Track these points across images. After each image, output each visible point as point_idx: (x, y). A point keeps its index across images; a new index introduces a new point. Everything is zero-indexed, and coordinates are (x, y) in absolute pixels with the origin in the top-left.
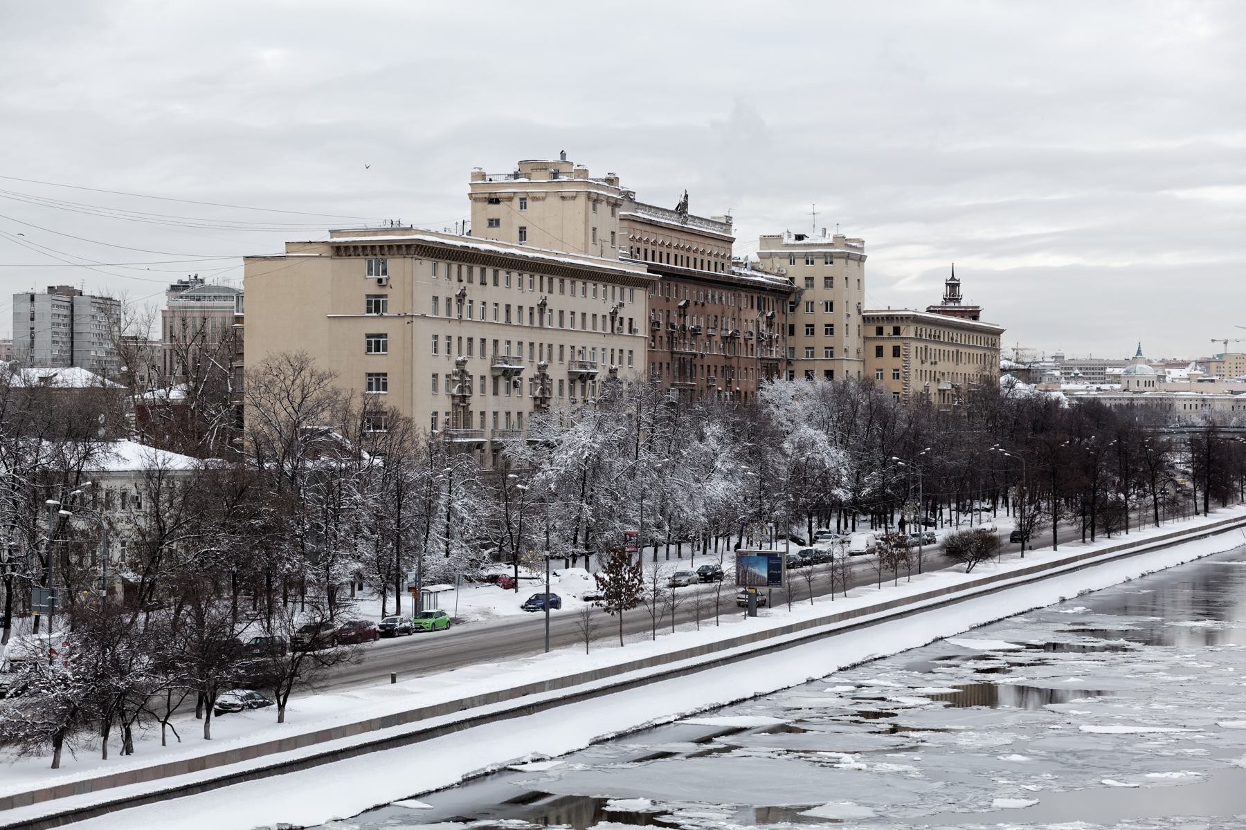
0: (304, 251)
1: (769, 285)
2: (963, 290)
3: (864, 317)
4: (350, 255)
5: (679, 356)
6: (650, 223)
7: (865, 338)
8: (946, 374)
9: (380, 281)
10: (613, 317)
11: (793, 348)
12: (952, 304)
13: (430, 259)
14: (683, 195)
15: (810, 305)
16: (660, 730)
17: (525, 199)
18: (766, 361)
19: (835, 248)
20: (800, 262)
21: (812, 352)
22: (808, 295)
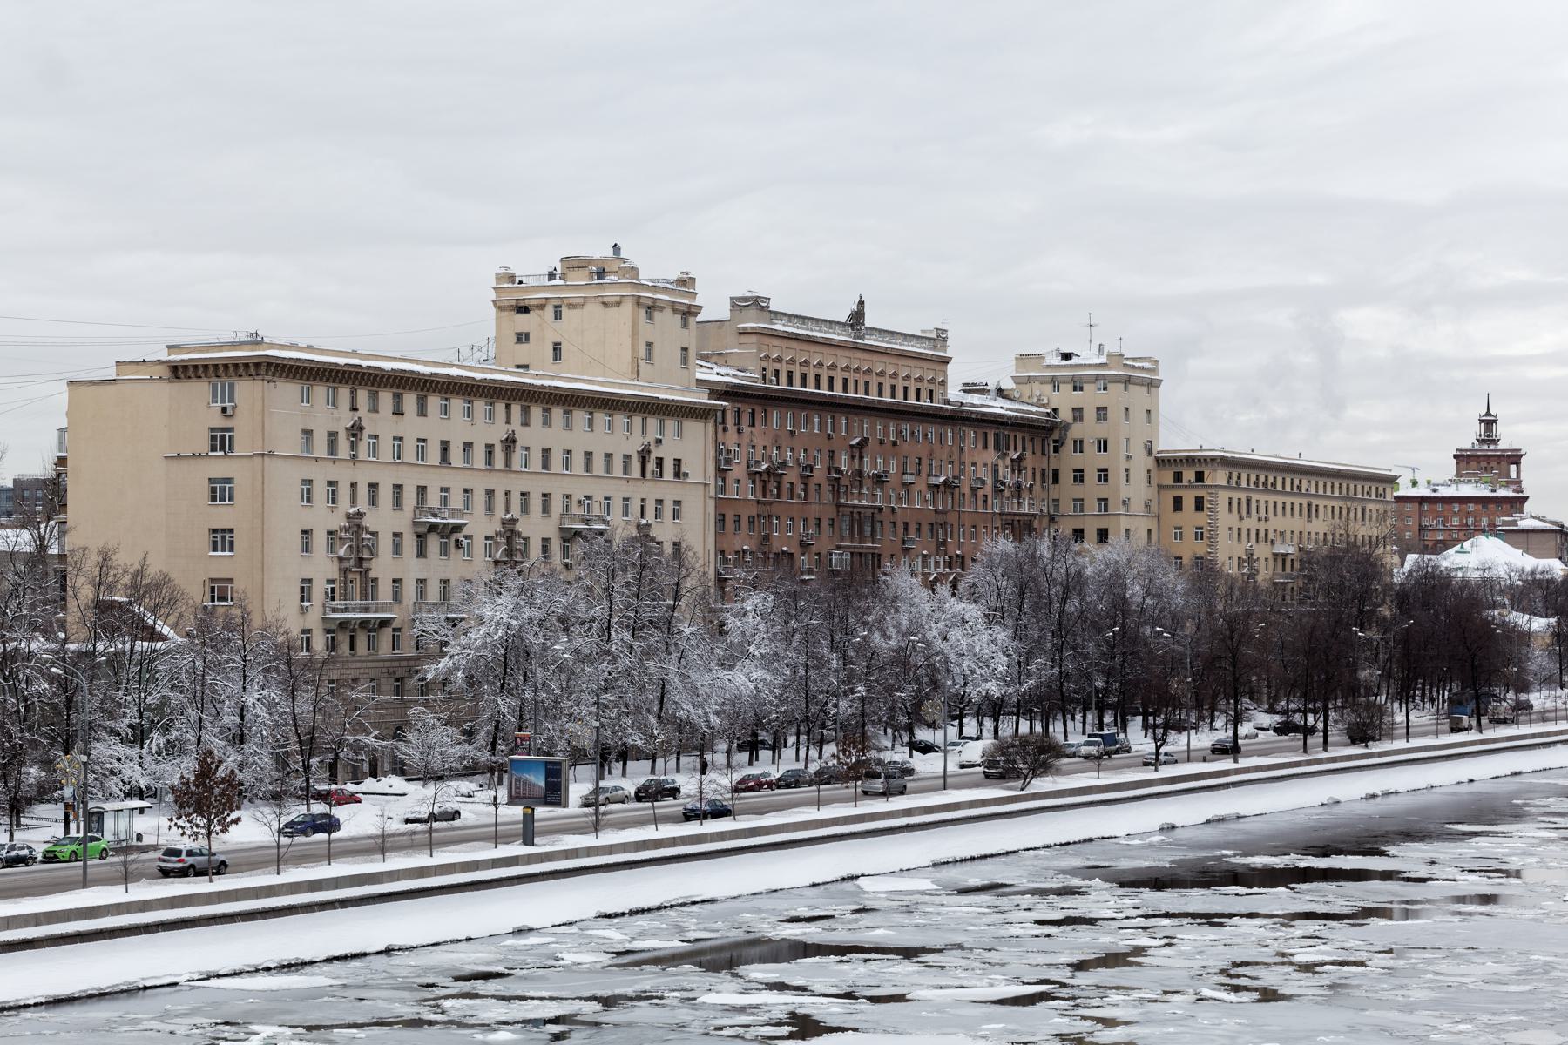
0: (137, 373)
1: (1010, 418)
2: (1500, 429)
3: (1157, 459)
4: (190, 377)
5: (851, 509)
6: (796, 338)
7: (1160, 487)
8: (1288, 535)
9: (224, 410)
10: (643, 458)
11: (1057, 500)
12: (1486, 447)
13: (295, 381)
14: (857, 301)
15: (1079, 445)
16: (157, 995)
17: (560, 306)
18: (1009, 517)
19: (1110, 369)
20: (1066, 388)
21: (1082, 506)
22: (1076, 432)
